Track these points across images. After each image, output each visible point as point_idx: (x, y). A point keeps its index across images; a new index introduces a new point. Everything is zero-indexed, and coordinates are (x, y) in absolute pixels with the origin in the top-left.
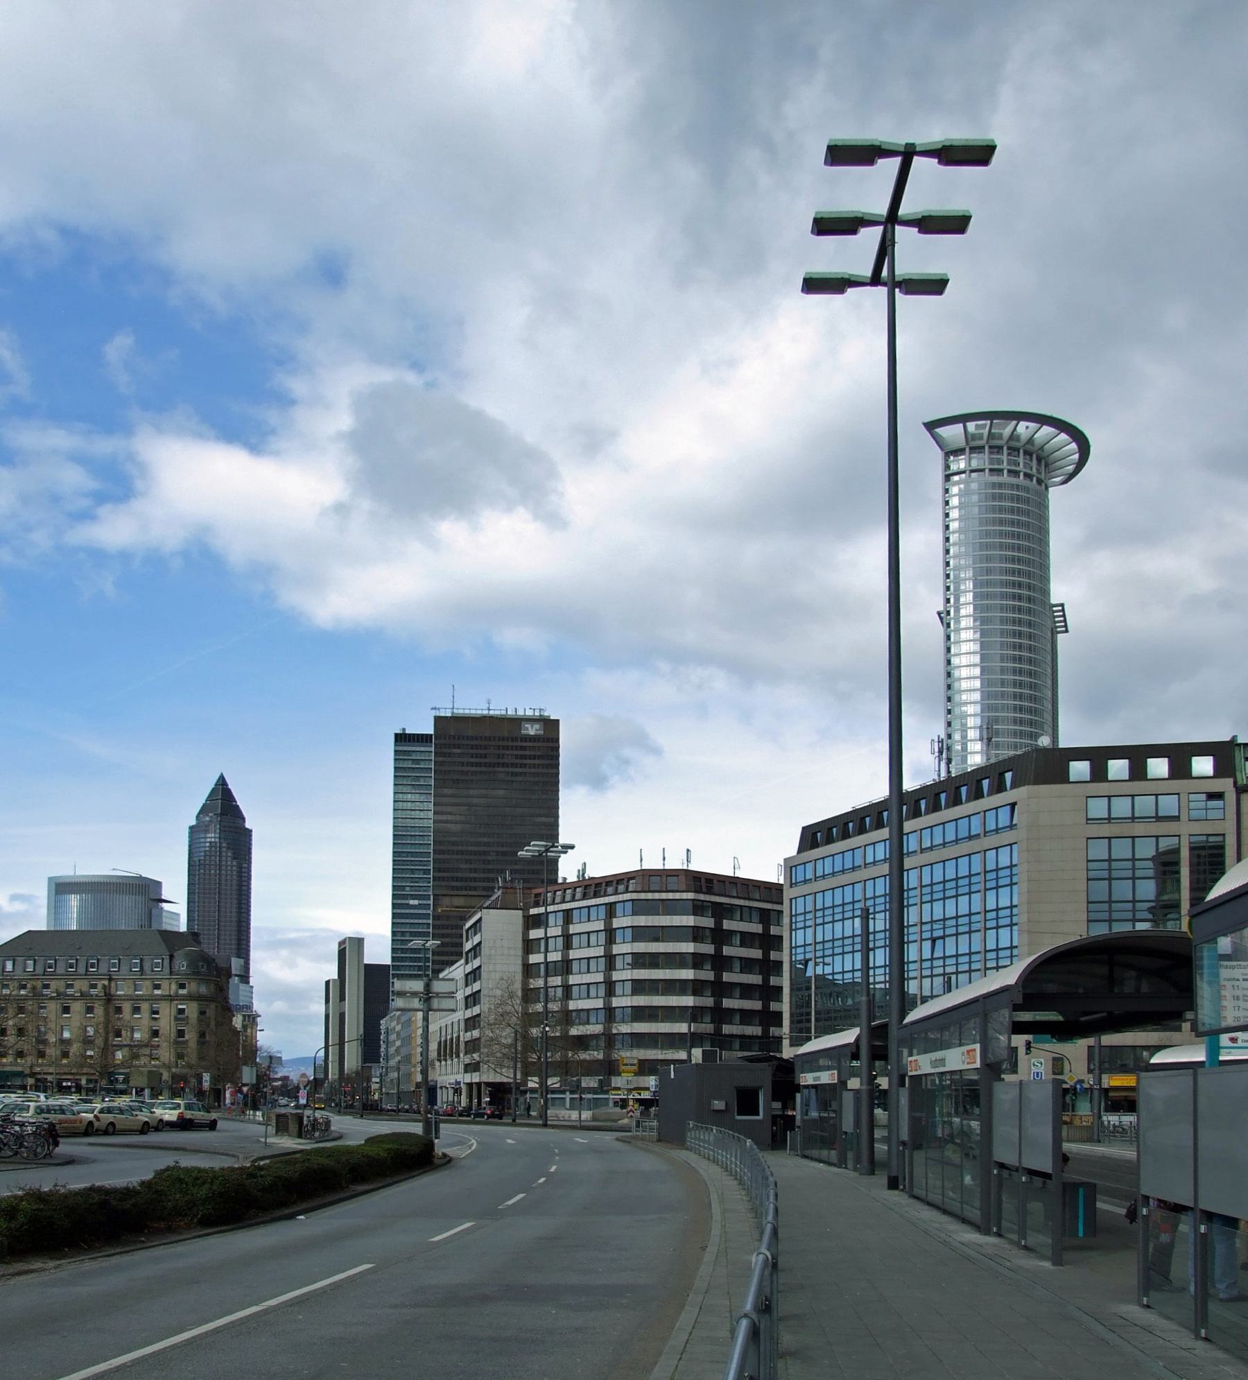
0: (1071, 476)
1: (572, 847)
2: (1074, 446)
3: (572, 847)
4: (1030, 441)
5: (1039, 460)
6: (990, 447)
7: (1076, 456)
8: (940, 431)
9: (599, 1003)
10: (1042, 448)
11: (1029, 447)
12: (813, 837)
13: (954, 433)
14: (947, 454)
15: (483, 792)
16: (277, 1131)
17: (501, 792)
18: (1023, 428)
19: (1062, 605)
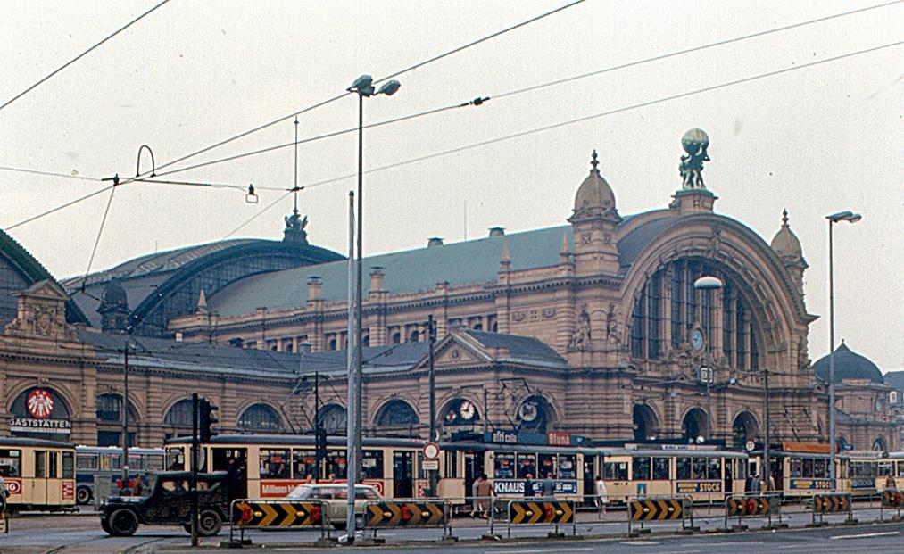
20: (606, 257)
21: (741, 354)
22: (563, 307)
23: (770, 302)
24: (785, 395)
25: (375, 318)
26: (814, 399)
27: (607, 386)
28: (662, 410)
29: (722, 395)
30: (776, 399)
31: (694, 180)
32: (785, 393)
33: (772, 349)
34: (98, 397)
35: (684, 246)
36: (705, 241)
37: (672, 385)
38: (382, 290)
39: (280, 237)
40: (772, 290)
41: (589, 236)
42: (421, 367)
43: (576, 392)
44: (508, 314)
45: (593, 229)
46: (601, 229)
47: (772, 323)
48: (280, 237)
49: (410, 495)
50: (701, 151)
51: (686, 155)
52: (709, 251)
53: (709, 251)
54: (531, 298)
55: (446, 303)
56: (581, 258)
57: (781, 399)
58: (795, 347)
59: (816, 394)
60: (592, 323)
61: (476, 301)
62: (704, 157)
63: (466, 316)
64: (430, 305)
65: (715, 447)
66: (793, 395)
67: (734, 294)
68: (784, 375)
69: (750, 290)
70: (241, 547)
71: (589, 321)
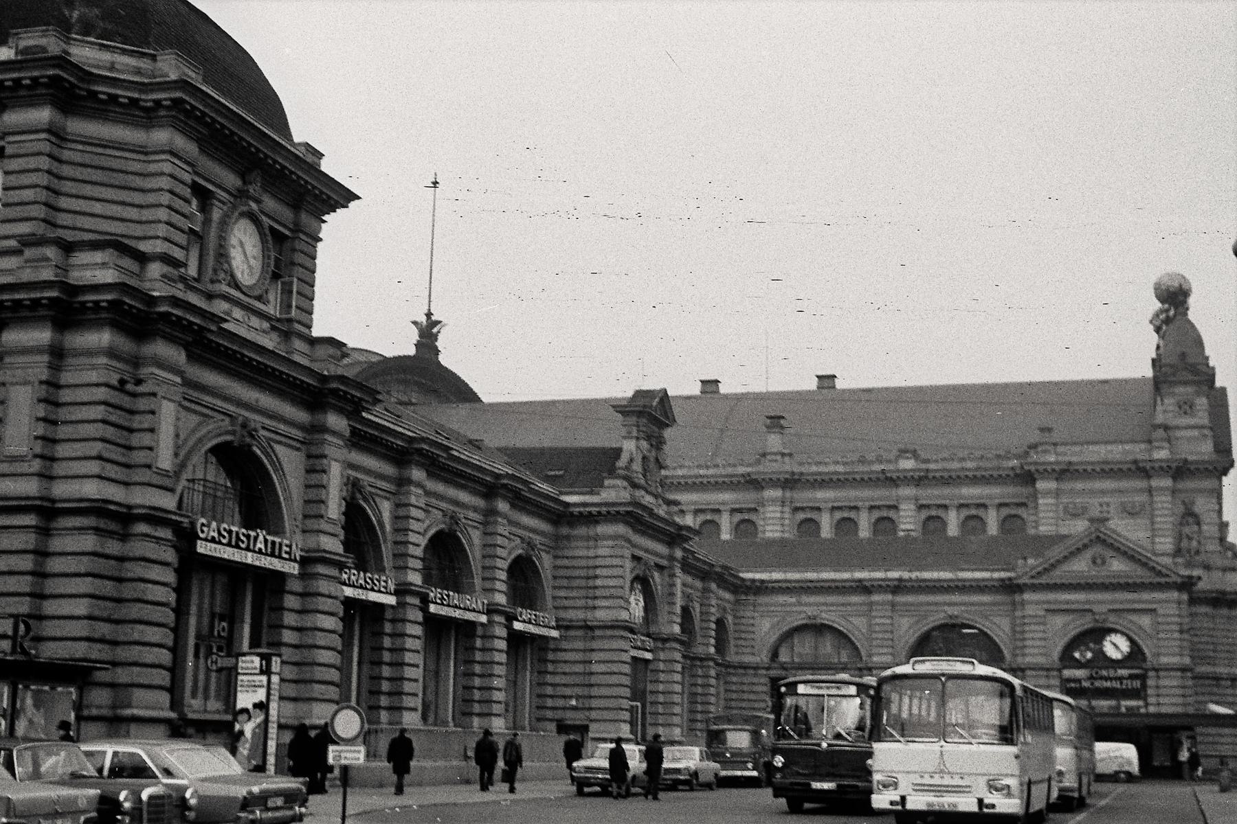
22: (1163, 501)
25: (776, 493)
34: (324, 471)
38: (786, 451)
39: (411, 351)
42: (1032, 577)
43: (570, 554)
44: (1057, 505)
45: (1198, 394)
48: (411, 351)
54: (1099, 485)
55: (920, 480)
56: (1179, 434)
60: (1205, 528)
61: (975, 480)
63: (867, 504)
64: (891, 481)
65: (135, 511)
70: (676, 790)
71: (1198, 524)
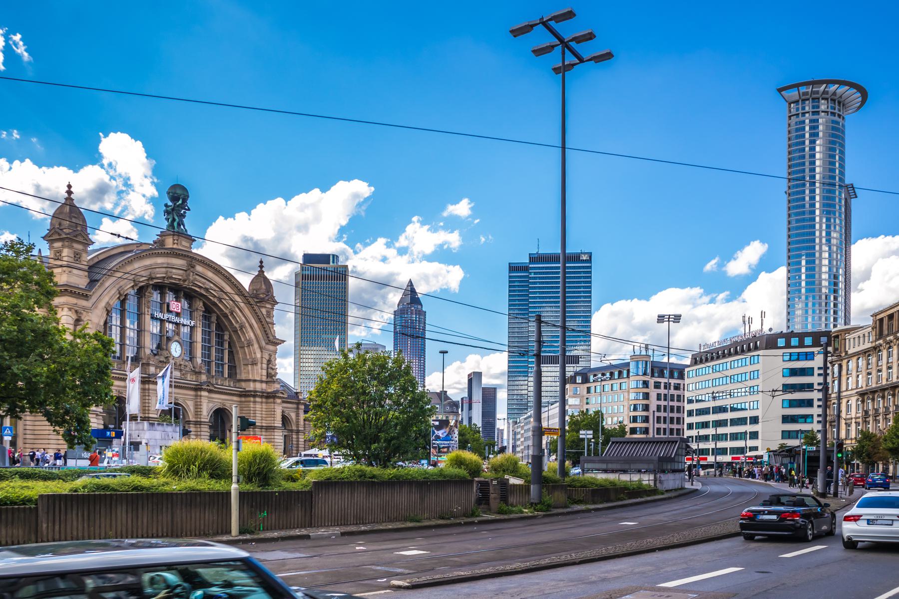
0: (859, 108)
1: (69, 186)
2: (859, 94)
3: (69, 186)
4: (834, 93)
5: (839, 103)
6: (813, 99)
7: (860, 99)
8: (783, 93)
9: (766, 303)
10: (841, 97)
11: (833, 97)
12: (534, 259)
13: (793, 94)
14: (790, 104)
15: (260, 335)
16: (516, 463)
17: (45, 526)
18: (833, 88)
19: (590, 255)
20: (75, 271)
21: (220, 366)
23: (242, 327)
24: (254, 396)
26: (279, 401)
27: (255, 402)
28: (192, 408)
29: (147, 386)
30: (248, 399)
31: (175, 224)
32: (254, 394)
33: (246, 362)
35: (160, 273)
36: (181, 272)
37: (201, 389)
40: (243, 316)
41: (60, 252)
45: (63, 246)
46: (71, 247)
47: (245, 342)
49: (228, 494)
50: (180, 202)
51: (170, 203)
52: (185, 281)
53: (185, 281)
57: (252, 399)
58: (265, 361)
59: (279, 398)
62: (183, 206)
66: (262, 397)
67: (214, 319)
68: (255, 381)
69: (226, 316)
